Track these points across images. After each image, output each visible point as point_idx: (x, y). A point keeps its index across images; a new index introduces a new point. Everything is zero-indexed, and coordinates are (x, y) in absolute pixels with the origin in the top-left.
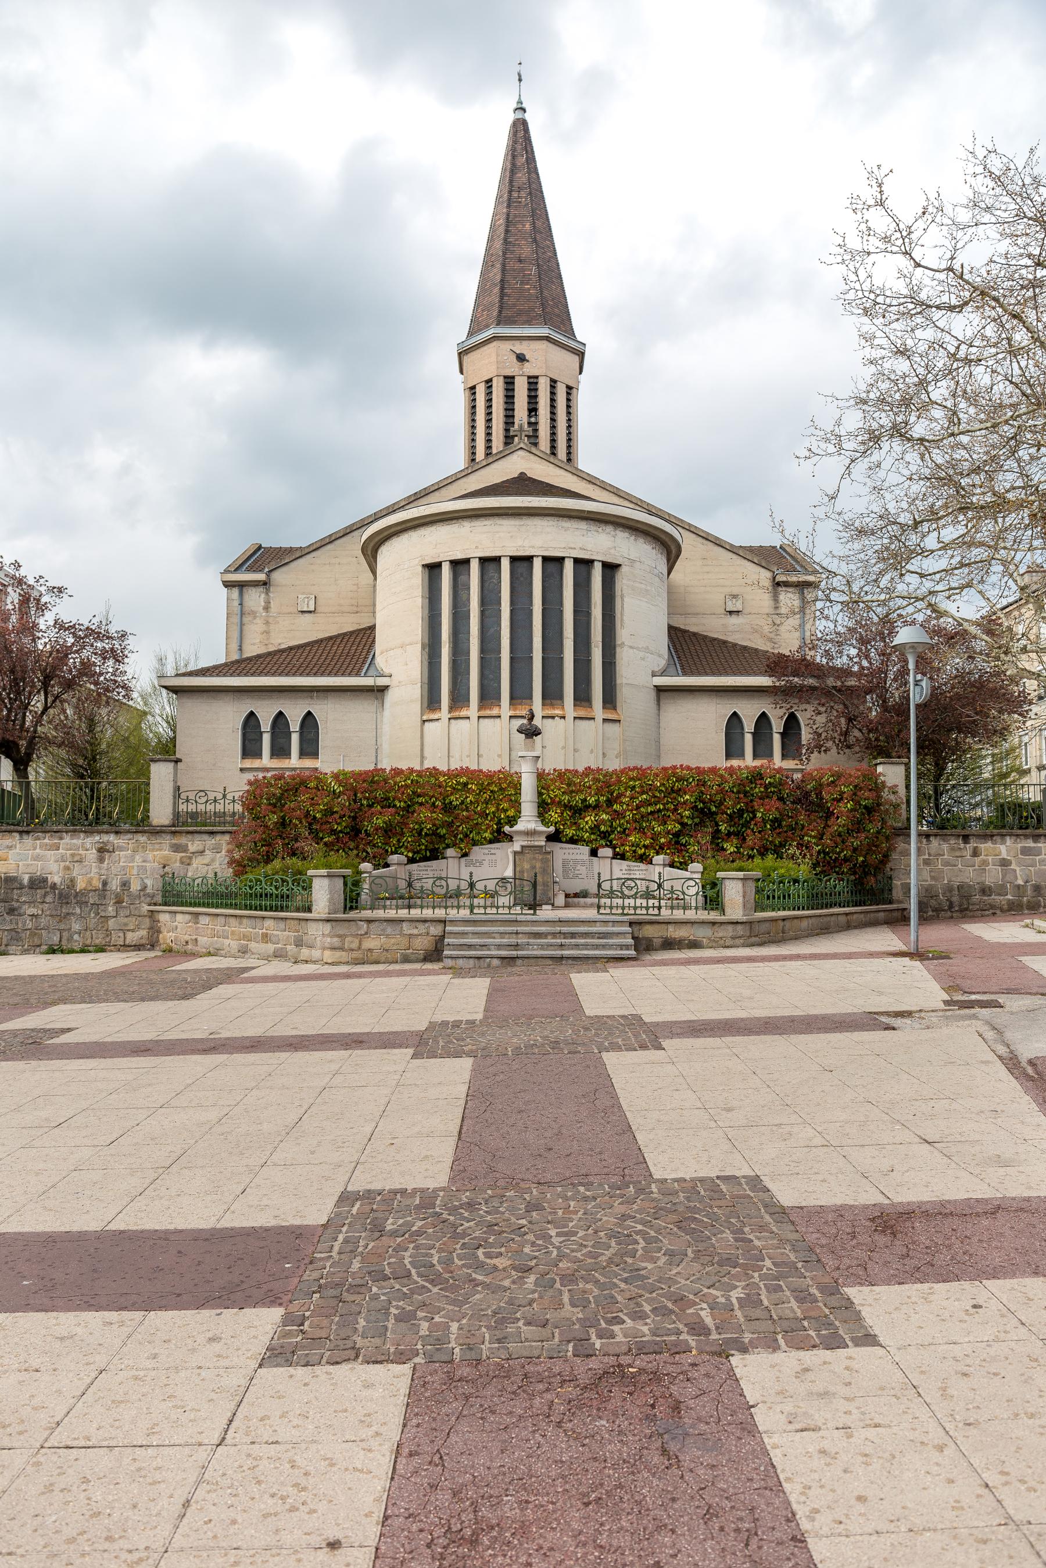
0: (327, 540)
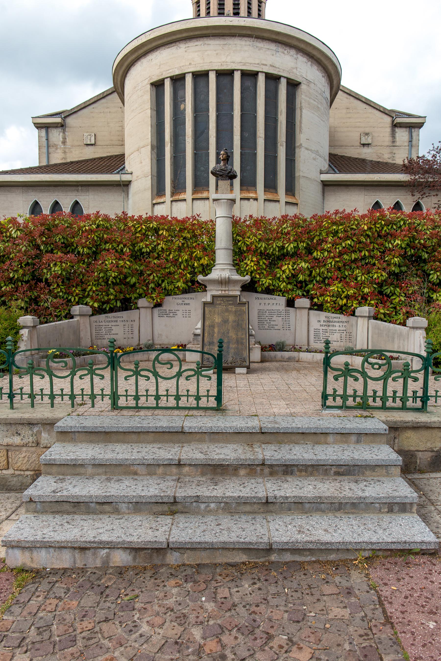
0: (102, 96)
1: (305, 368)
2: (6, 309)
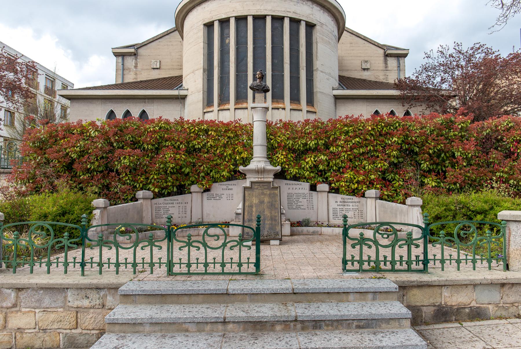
0: (166, 33)
1: (327, 240)
2: (83, 193)
